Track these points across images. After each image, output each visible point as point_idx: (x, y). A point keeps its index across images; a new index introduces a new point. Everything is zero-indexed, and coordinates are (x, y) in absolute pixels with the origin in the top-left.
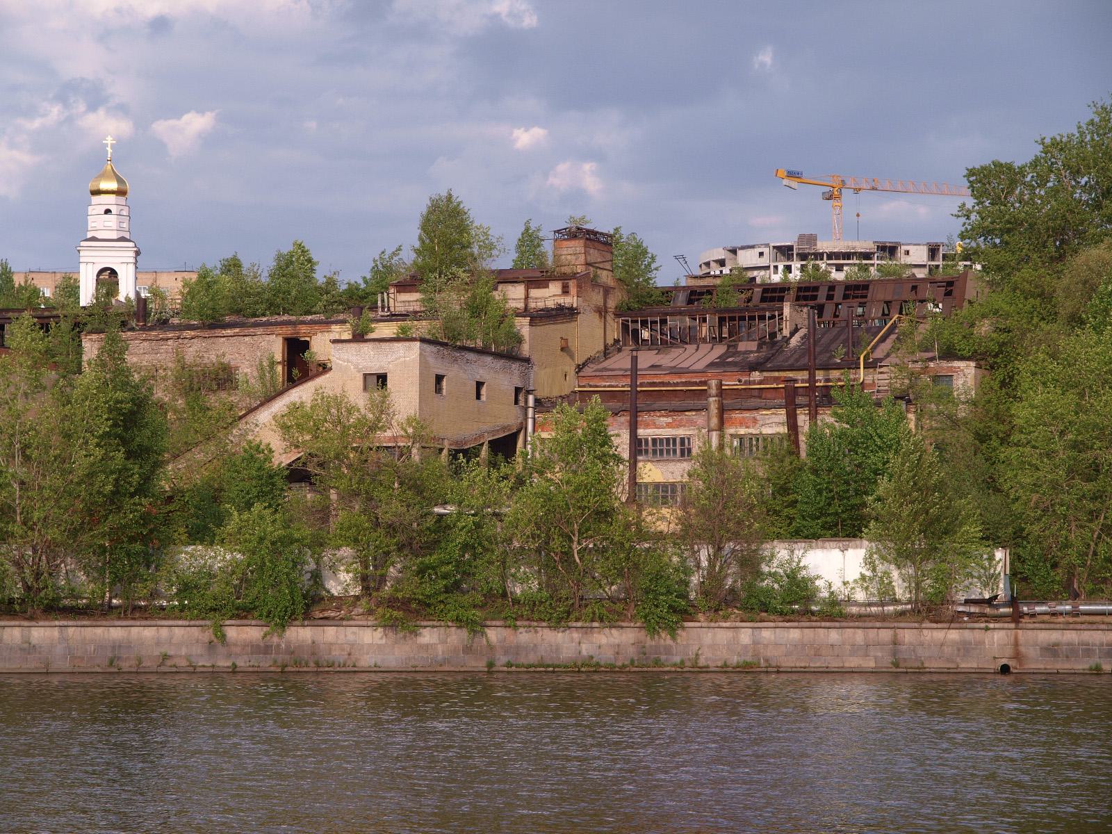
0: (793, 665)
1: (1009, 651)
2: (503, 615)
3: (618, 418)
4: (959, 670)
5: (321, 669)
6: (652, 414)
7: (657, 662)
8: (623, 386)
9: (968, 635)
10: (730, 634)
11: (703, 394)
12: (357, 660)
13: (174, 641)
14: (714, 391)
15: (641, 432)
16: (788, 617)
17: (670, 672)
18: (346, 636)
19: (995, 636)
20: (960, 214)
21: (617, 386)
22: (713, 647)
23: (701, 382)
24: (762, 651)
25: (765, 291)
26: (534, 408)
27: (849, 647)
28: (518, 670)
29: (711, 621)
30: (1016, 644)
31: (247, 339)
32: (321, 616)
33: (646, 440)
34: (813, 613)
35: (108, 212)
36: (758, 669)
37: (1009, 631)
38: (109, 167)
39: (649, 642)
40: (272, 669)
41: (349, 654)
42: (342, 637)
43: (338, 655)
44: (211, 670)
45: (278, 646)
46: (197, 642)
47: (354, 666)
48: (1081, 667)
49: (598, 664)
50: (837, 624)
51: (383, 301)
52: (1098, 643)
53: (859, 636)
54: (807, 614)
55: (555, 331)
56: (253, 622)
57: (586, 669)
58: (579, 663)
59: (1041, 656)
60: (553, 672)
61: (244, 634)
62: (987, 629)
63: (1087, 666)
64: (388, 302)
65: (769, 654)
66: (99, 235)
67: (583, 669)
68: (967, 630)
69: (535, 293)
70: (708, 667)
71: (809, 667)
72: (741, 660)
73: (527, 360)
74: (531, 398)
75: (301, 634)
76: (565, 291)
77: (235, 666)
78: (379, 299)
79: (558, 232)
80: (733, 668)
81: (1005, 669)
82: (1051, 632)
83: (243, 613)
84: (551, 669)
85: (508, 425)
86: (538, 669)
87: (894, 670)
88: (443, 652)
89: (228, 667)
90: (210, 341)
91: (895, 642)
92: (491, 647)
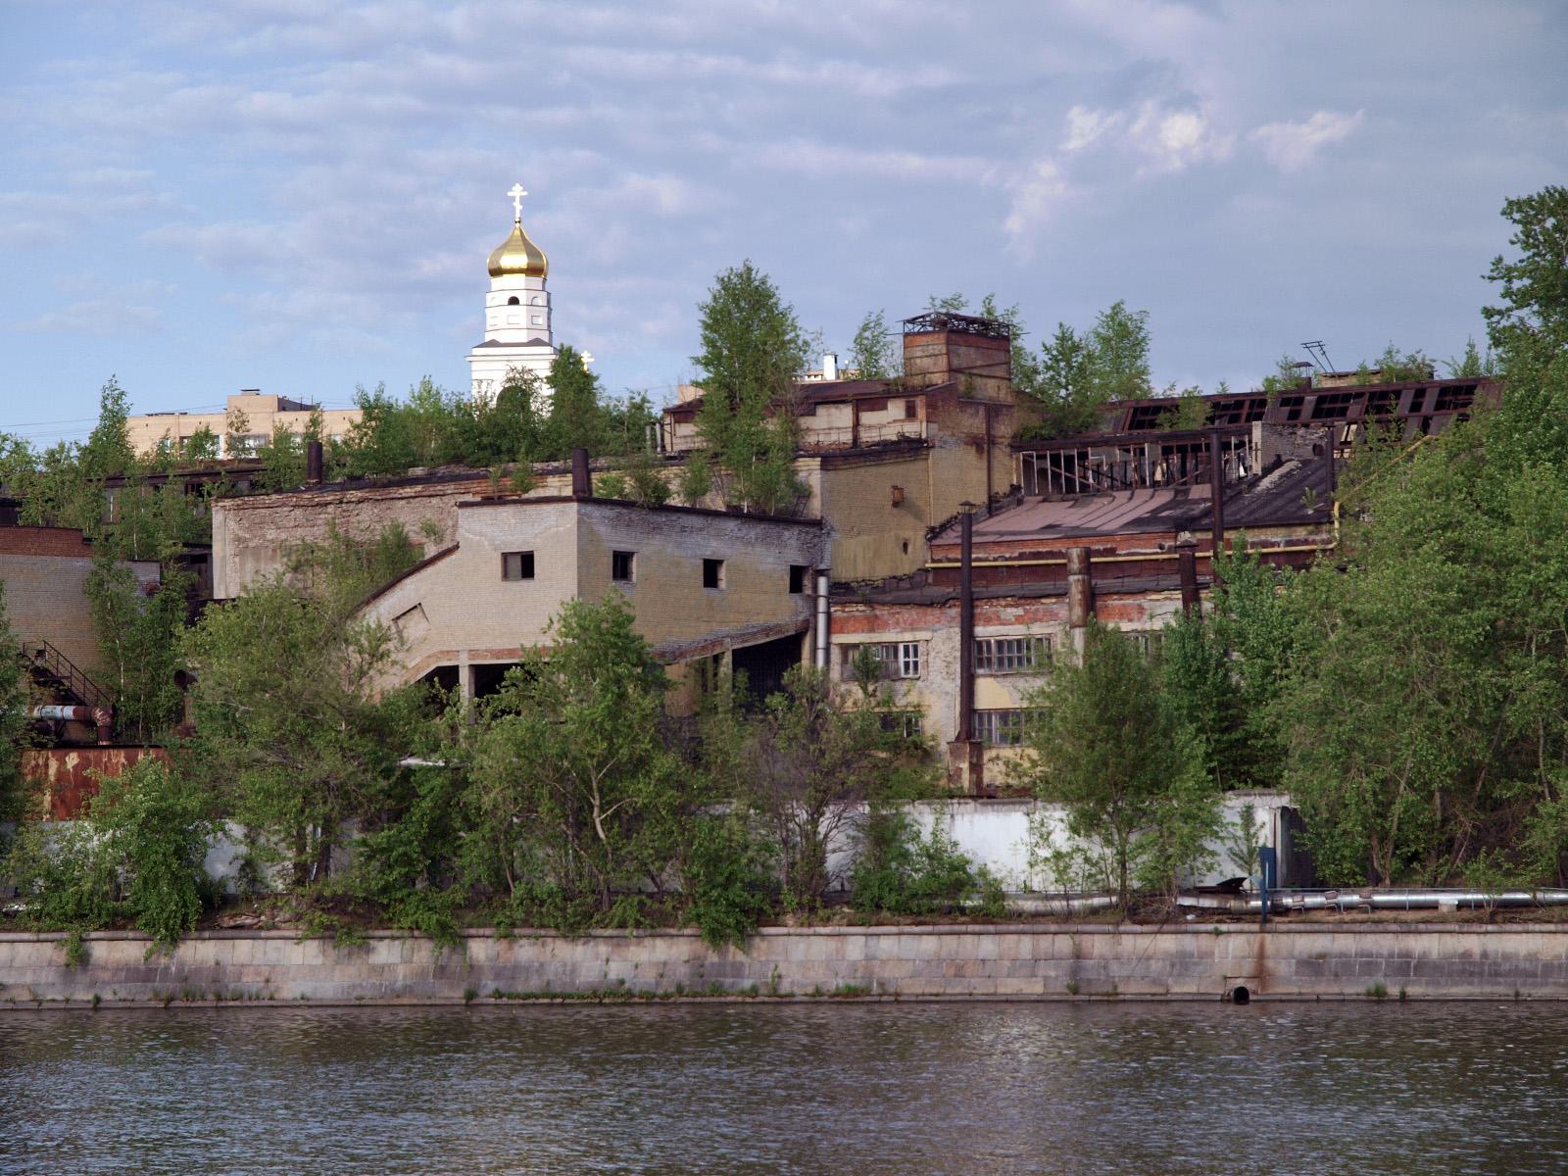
0: (920, 991)
1: (1248, 967)
2: (496, 921)
3: (948, 611)
4: (1169, 997)
5: (222, 1004)
6: (995, 602)
7: (718, 990)
8: (995, 560)
9: (1189, 943)
10: (832, 944)
11: (1062, 571)
12: (277, 989)
13: (17, 963)
14: (1075, 565)
15: (981, 631)
16: (922, 918)
17: (735, 1003)
18: (265, 953)
19: (1231, 945)
20: (1495, 274)
21: (986, 560)
22: (804, 965)
23: (1105, 550)
24: (877, 970)
25: (1321, 400)
26: (827, 598)
27: (1007, 963)
28: (511, 1002)
29: (802, 925)
30: (1261, 956)
31: (434, 501)
32: (232, 923)
33: (988, 643)
34: (962, 911)
35: (514, 301)
36: (868, 999)
37: (1252, 936)
38: (517, 232)
39: (713, 958)
40: (153, 1004)
41: (267, 981)
42: (259, 955)
43: (251, 982)
44: (62, 1006)
45: (167, 968)
46: (49, 965)
47: (271, 998)
48: (1352, 991)
49: (630, 994)
50: (991, 928)
51: (654, 436)
52: (1385, 952)
53: (1025, 946)
54: (955, 913)
55: (880, 479)
56: (131, 935)
57: (618, 996)
58: (601, 992)
59: (1297, 973)
60: (562, 1005)
61: (118, 952)
62: (1218, 933)
63: (1362, 989)
64: (662, 436)
65: (886, 975)
66: (502, 338)
67: (606, 1001)
68: (1189, 936)
69: (867, 418)
70: (792, 995)
71: (944, 994)
72: (841, 983)
73: (818, 524)
74: (822, 582)
75: (200, 952)
76: (911, 413)
77: (98, 1000)
78: (648, 432)
79: (913, 321)
80: (831, 996)
81: (1241, 996)
82: (1315, 936)
83: (118, 922)
84: (559, 1000)
85: (777, 626)
86: (541, 1001)
87: (1071, 997)
88: (405, 976)
89: (89, 1002)
90: (384, 506)
91: (1078, 955)
92: (473, 968)
